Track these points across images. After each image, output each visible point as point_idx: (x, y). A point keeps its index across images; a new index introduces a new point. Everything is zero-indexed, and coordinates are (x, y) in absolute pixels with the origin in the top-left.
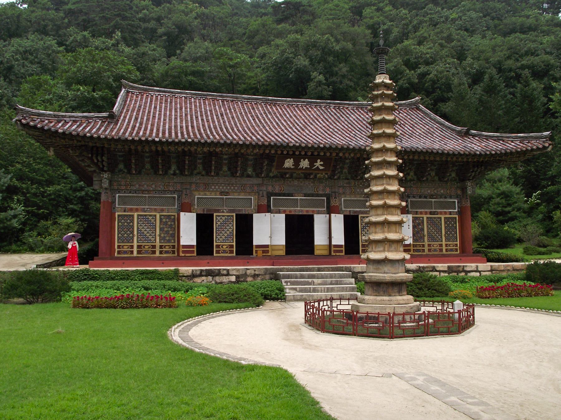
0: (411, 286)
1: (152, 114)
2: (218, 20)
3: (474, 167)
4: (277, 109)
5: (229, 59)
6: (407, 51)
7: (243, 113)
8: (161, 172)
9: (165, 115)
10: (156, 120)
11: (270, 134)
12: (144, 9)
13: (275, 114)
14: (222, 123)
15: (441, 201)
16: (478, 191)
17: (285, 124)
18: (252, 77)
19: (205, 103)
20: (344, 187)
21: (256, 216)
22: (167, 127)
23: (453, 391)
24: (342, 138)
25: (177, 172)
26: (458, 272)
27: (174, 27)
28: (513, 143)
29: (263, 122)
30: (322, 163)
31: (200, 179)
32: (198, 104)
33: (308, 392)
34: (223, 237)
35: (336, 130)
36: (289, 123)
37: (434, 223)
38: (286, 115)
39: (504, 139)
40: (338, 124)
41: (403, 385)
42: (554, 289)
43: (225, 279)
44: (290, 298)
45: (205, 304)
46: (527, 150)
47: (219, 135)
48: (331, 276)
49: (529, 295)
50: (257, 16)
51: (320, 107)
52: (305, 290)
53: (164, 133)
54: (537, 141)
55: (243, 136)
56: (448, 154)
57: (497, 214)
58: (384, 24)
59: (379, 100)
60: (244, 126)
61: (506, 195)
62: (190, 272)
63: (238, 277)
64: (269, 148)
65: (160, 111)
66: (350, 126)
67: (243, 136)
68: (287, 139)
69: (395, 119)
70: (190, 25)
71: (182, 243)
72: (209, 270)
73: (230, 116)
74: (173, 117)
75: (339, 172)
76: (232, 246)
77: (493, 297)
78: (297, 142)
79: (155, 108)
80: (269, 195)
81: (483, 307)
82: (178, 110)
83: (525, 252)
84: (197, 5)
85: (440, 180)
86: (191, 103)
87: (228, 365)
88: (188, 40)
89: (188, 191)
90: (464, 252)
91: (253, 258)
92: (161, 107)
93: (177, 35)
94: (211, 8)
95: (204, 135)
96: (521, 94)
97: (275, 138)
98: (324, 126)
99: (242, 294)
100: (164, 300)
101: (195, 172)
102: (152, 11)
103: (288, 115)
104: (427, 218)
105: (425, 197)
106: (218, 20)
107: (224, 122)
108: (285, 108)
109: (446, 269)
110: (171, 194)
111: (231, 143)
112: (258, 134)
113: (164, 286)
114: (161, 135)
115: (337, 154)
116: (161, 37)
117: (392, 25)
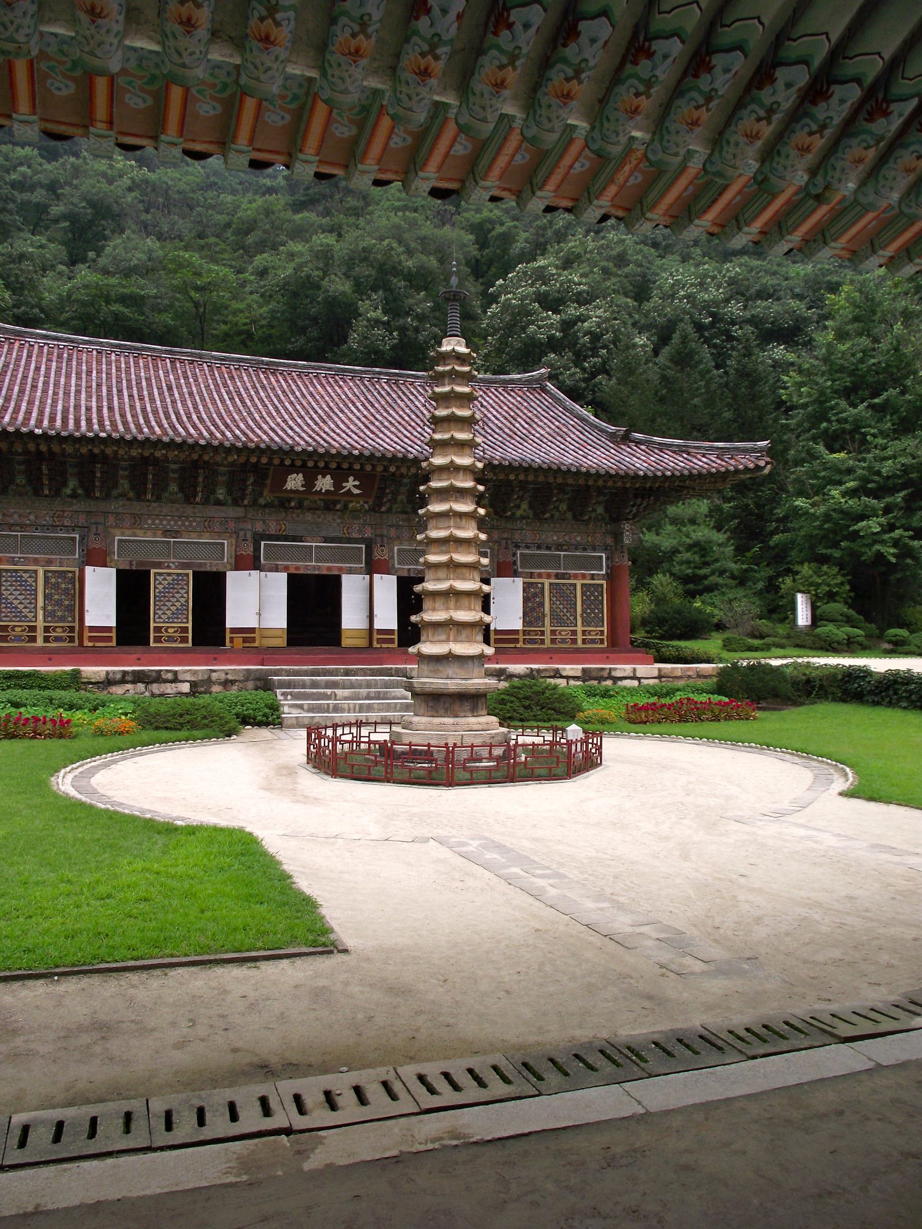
0: (512, 702)
1: (30, 380)
2: (177, 196)
3: (636, 496)
4: (278, 381)
5: (195, 274)
6: (541, 276)
7: (212, 387)
8: (46, 492)
9: (57, 384)
10: (39, 394)
11: (260, 428)
12: (21, 164)
13: (273, 389)
14: (169, 403)
15: (577, 556)
16: (650, 538)
17: (291, 409)
18: (241, 311)
19: (137, 364)
20: (398, 527)
21: (232, 577)
22: (60, 407)
23: (520, 859)
24: (396, 439)
25: (80, 491)
26: (600, 679)
27: (84, 204)
28: (704, 458)
29: (249, 404)
30: (357, 483)
31: (124, 505)
32: (123, 365)
33: (279, 863)
34: (169, 612)
35: (386, 424)
36: (298, 407)
37: (563, 594)
38: (293, 393)
39: (691, 450)
40: (391, 412)
41: (444, 853)
42: (759, 709)
43: (169, 689)
44: (290, 722)
45: (127, 732)
46: (728, 471)
47: (161, 426)
48: (369, 685)
49: (716, 719)
50: (256, 192)
51: (361, 379)
52: (319, 709)
53: (52, 419)
54: (748, 456)
55: (208, 430)
56: (588, 474)
57: (686, 580)
58: (502, 224)
59: (446, 381)
60: (212, 410)
61: (701, 548)
62: (103, 675)
63: (193, 685)
64: (257, 454)
65: (47, 376)
66: (413, 417)
67: (208, 430)
68: (291, 437)
69: (473, 416)
70: (116, 202)
71: (89, 621)
72: (139, 672)
73: (185, 390)
74: (73, 389)
75: (389, 501)
76: (185, 630)
77: (653, 721)
78: (310, 445)
79: (38, 369)
80: (258, 538)
81: (631, 738)
82: (84, 376)
83: (724, 646)
84: (133, 162)
85: (575, 518)
86: (109, 364)
87: (152, 827)
88: (113, 232)
89: (100, 527)
90: (618, 644)
91: (226, 651)
92: (48, 369)
93: (90, 221)
94: (161, 171)
95: (132, 426)
96: (736, 370)
97: (268, 436)
98: (365, 417)
99: (198, 715)
100: (49, 725)
101: (115, 493)
102: (39, 168)
103: (297, 393)
104: (551, 584)
105: (548, 548)
106: (177, 196)
107: (174, 402)
108: (293, 379)
109: (579, 674)
110: (68, 532)
111: (184, 442)
112: (238, 427)
113: (51, 700)
114: (46, 423)
115: (386, 469)
116: (56, 221)
117: (515, 227)
